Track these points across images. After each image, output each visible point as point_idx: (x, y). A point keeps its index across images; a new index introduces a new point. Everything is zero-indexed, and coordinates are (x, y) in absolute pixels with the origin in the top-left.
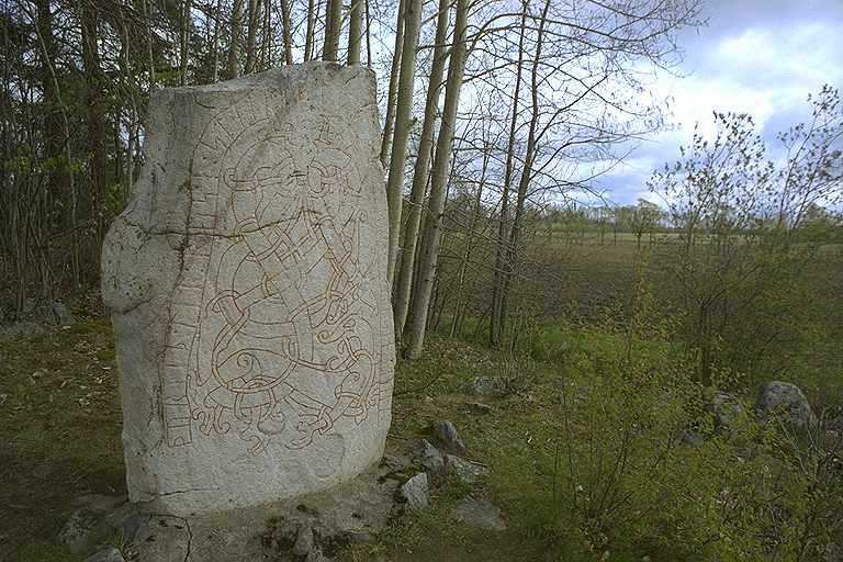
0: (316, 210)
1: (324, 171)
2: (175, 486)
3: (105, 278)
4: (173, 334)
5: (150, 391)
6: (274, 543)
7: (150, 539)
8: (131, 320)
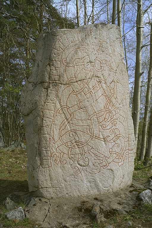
0: (99, 76)
1: (101, 61)
2: (45, 185)
4: (44, 121)
5: (36, 145)
6: (83, 210)
7: (34, 205)
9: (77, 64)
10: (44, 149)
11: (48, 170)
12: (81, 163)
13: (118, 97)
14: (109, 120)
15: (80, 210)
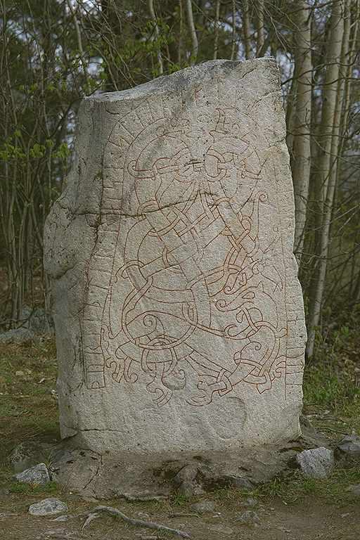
0: (213, 192)
1: (221, 157)
2: (92, 424)
3: (46, 250)
5: (74, 342)
6: (163, 474)
7: (69, 462)
8: (62, 283)
9: (161, 171)
10: (91, 351)
11: (98, 394)
12: (167, 380)
13: (261, 237)
14: (234, 290)
15: (157, 473)
